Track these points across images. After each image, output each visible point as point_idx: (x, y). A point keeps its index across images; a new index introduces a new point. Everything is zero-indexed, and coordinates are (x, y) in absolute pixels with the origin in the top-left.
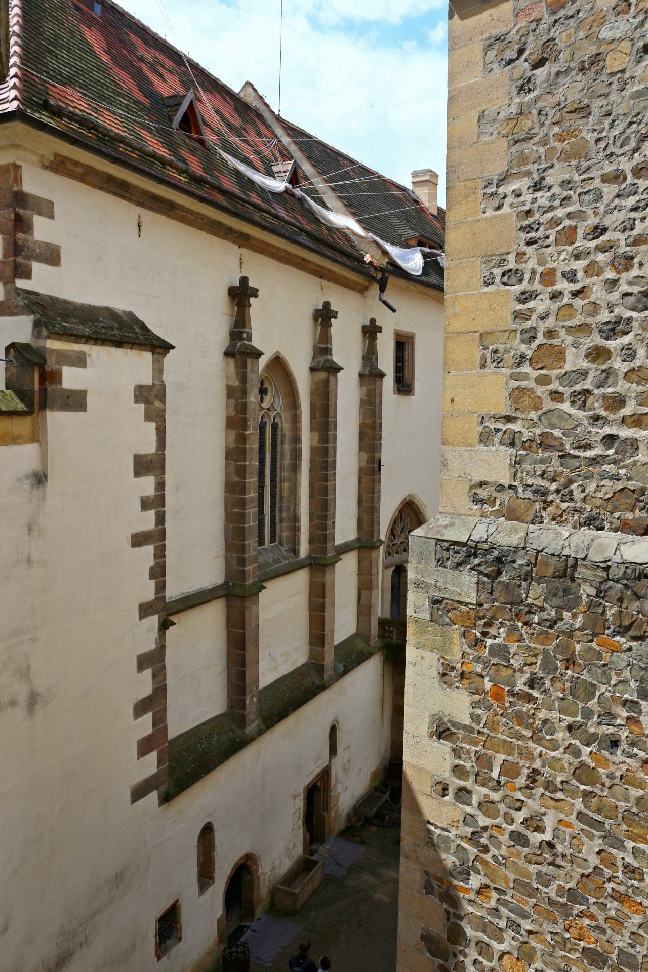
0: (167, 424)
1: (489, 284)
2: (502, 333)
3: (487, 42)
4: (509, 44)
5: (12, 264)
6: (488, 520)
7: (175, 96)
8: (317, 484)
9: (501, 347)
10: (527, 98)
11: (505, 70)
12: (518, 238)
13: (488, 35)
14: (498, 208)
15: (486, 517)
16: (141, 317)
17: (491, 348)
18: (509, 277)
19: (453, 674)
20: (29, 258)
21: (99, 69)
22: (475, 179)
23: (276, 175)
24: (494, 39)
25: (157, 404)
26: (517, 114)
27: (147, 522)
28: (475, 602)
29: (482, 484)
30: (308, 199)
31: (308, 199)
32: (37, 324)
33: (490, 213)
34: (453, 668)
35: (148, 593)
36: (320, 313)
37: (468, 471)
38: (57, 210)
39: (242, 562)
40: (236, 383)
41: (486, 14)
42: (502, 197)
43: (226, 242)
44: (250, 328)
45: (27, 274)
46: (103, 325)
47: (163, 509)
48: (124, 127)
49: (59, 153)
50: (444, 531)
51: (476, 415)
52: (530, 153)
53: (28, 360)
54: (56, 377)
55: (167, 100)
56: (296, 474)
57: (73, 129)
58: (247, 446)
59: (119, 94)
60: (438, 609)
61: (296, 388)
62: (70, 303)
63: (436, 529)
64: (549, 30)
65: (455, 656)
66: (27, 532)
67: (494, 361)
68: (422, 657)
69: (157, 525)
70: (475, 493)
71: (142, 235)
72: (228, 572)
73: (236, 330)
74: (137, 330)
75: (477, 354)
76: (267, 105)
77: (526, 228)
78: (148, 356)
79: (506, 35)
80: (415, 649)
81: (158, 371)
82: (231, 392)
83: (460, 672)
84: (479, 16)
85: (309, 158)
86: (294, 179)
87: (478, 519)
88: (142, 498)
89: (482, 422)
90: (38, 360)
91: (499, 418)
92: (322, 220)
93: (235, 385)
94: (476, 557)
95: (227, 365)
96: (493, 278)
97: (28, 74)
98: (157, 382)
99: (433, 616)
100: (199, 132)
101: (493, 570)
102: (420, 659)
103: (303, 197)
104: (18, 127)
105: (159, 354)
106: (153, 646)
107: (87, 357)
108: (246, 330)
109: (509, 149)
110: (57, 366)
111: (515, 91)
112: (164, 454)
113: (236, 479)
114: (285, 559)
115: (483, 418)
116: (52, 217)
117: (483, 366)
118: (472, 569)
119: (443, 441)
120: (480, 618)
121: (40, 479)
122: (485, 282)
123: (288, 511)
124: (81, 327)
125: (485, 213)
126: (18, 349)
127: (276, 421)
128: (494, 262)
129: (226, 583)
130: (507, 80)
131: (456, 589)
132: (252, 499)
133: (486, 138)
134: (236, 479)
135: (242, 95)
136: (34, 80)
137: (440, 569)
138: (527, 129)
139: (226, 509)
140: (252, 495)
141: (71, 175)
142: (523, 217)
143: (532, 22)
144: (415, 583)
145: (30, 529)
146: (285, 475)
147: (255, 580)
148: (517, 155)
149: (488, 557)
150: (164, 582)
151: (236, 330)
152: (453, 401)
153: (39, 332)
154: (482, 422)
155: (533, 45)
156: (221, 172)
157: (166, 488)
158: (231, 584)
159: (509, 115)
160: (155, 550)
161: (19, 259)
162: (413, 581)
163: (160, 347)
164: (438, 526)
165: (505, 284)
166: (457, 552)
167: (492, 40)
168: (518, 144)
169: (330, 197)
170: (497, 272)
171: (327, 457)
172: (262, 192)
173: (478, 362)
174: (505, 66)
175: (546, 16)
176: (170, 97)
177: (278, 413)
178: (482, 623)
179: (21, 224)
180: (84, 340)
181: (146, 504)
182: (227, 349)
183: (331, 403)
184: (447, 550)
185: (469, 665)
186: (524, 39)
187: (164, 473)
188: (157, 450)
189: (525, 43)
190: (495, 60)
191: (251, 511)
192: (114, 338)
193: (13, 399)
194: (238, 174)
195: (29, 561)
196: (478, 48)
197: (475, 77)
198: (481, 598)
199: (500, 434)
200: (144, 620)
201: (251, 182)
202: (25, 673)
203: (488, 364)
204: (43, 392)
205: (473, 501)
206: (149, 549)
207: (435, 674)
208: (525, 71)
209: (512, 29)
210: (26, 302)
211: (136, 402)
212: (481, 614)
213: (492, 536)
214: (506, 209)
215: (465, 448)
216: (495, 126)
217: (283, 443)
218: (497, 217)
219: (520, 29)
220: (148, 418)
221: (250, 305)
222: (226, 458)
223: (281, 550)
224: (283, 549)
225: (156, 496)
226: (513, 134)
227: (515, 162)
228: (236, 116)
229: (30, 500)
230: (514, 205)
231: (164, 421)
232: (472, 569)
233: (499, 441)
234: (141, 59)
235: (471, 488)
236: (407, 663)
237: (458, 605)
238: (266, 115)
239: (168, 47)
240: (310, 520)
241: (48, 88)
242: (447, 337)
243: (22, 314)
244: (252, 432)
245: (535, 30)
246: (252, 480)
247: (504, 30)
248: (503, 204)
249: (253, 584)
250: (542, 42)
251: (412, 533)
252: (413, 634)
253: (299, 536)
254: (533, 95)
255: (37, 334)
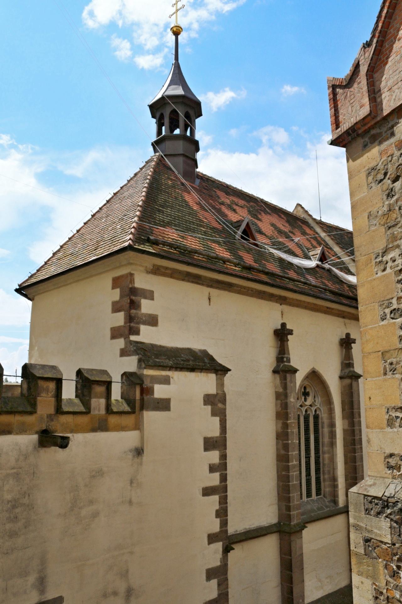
0: (227, 418)
1: (384, 319)
2: (394, 351)
3: (367, 172)
4: (379, 171)
5: (128, 328)
6: (397, 481)
7: (239, 221)
8: (349, 455)
9: (394, 360)
10: (392, 201)
11: (378, 186)
12: (397, 288)
13: (367, 168)
14: (384, 270)
15: (395, 479)
16: (211, 352)
17: (388, 361)
18: (394, 314)
19: (382, 598)
20: (138, 323)
21: (190, 214)
22: (369, 254)
23: (312, 257)
24: (371, 169)
25: (220, 405)
26: (388, 211)
27: (214, 479)
28: (390, 542)
29: (391, 455)
30: (334, 269)
31: (334, 269)
32: (140, 361)
33: (380, 274)
34: (381, 593)
35: (215, 526)
36: (344, 341)
37: (382, 446)
38: (156, 295)
39: (289, 509)
40: (281, 390)
41: (365, 156)
42: (385, 263)
43: (270, 302)
44: (289, 354)
45: (137, 333)
46: (182, 359)
47: (225, 472)
48: (201, 244)
49: (156, 264)
50: (369, 489)
51: (384, 407)
52: (398, 233)
53: (132, 381)
54: (150, 391)
55: (234, 224)
56: (333, 448)
57: (165, 250)
58: (289, 430)
59: (201, 226)
60: (369, 546)
61: (330, 391)
62: (163, 347)
63: (365, 487)
64: (399, 159)
65: (382, 584)
66: (129, 484)
67: (391, 370)
68: (362, 583)
69: (221, 482)
70: (388, 462)
71: (212, 303)
72: (280, 516)
73: (280, 356)
74: (206, 360)
75: (381, 365)
76: (310, 216)
77: (400, 281)
78: (212, 377)
79: (377, 166)
80: (357, 575)
81: (220, 385)
82: (278, 396)
83: (386, 596)
84: (362, 158)
85: (338, 244)
86: (323, 258)
87: (391, 480)
88: (210, 465)
89: (388, 412)
90: (138, 381)
91: (398, 409)
92: (344, 281)
93: (280, 391)
94: (388, 508)
95: (275, 378)
96: (386, 315)
97: (142, 225)
98: (220, 392)
99: (366, 551)
100: (254, 239)
101: (399, 518)
102: (361, 583)
103: (330, 268)
104: (131, 253)
105: (221, 375)
106: (219, 564)
107: (171, 379)
108: (286, 356)
109: (386, 233)
110: (151, 385)
111: (385, 197)
112: (226, 437)
113: (283, 452)
114: (327, 507)
115: (388, 409)
116: (153, 299)
117: (385, 374)
118: (387, 517)
119: (367, 426)
120: (395, 554)
121: (139, 452)
122: (381, 318)
123: (329, 473)
124: (167, 361)
125: (377, 274)
126: (127, 376)
127: (317, 413)
128: (385, 305)
129: (279, 523)
130: (380, 192)
131: (378, 532)
132: (294, 466)
133: (373, 228)
134: (283, 452)
135: (295, 213)
136: (145, 227)
137: (367, 516)
138: (394, 219)
139: (278, 472)
140: (295, 463)
141: (164, 275)
142: (398, 274)
143: (389, 156)
144: (354, 526)
145: (131, 482)
146: (326, 449)
147: (299, 521)
148: (391, 235)
149: (395, 508)
150: (227, 520)
151: (280, 356)
152: (370, 398)
153: (140, 365)
154: (388, 412)
155: (391, 170)
156: (267, 261)
157: (227, 459)
158: (282, 524)
159: (384, 213)
160: (220, 498)
161: (132, 324)
162: (353, 525)
163: (221, 370)
164: (366, 485)
165: (393, 318)
166: (377, 504)
167: (370, 170)
168: (391, 229)
169: (353, 266)
170: (388, 311)
171: (354, 436)
172: (299, 270)
173: (382, 371)
174: (378, 184)
175: (396, 152)
176: (236, 222)
177: (318, 408)
178: (396, 559)
179: (134, 305)
180: (168, 368)
181: (212, 469)
182: (274, 368)
183: (355, 399)
184: (371, 502)
185: (391, 591)
186: (386, 167)
187: (226, 449)
188: (221, 434)
189: (387, 169)
190: (373, 181)
191: (294, 473)
192: (188, 367)
193: (123, 404)
194: (281, 260)
195: (130, 502)
196: (363, 175)
197: (363, 193)
198: (394, 539)
199: (399, 420)
200: (212, 546)
201: (291, 264)
202: (125, 574)
203: (388, 372)
204: (142, 400)
205: (388, 468)
206: (216, 498)
207: (371, 597)
208: (389, 185)
209: (379, 162)
210: (135, 348)
211: (205, 404)
212: (395, 551)
213: (398, 493)
214: (388, 270)
215: (379, 430)
216: (377, 220)
217: (323, 427)
218: (384, 276)
219: (383, 161)
220: (214, 414)
221: (288, 340)
222: (277, 439)
223: (324, 501)
224: (326, 500)
225: (220, 464)
226: (387, 223)
227: (390, 240)
228: (287, 225)
229: (132, 465)
230: (393, 267)
231: (225, 416)
232: (387, 517)
233: (398, 425)
234: (222, 204)
235: (385, 458)
236: (353, 587)
237: (380, 544)
238: (310, 221)
239: (242, 194)
240: (346, 480)
241: (153, 230)
242: (364, 356)
243: (133, 355)
244: (292, 421)
245: (391, 161)
246: (294, 453)
247: (375, 164)
248: (386, 267)
249: (298, 524)
250: (396, 167)
251: (350, 490)
252: (355, 564)
253: (337, 491)
254: (395, 198)
255: (139, 367)
